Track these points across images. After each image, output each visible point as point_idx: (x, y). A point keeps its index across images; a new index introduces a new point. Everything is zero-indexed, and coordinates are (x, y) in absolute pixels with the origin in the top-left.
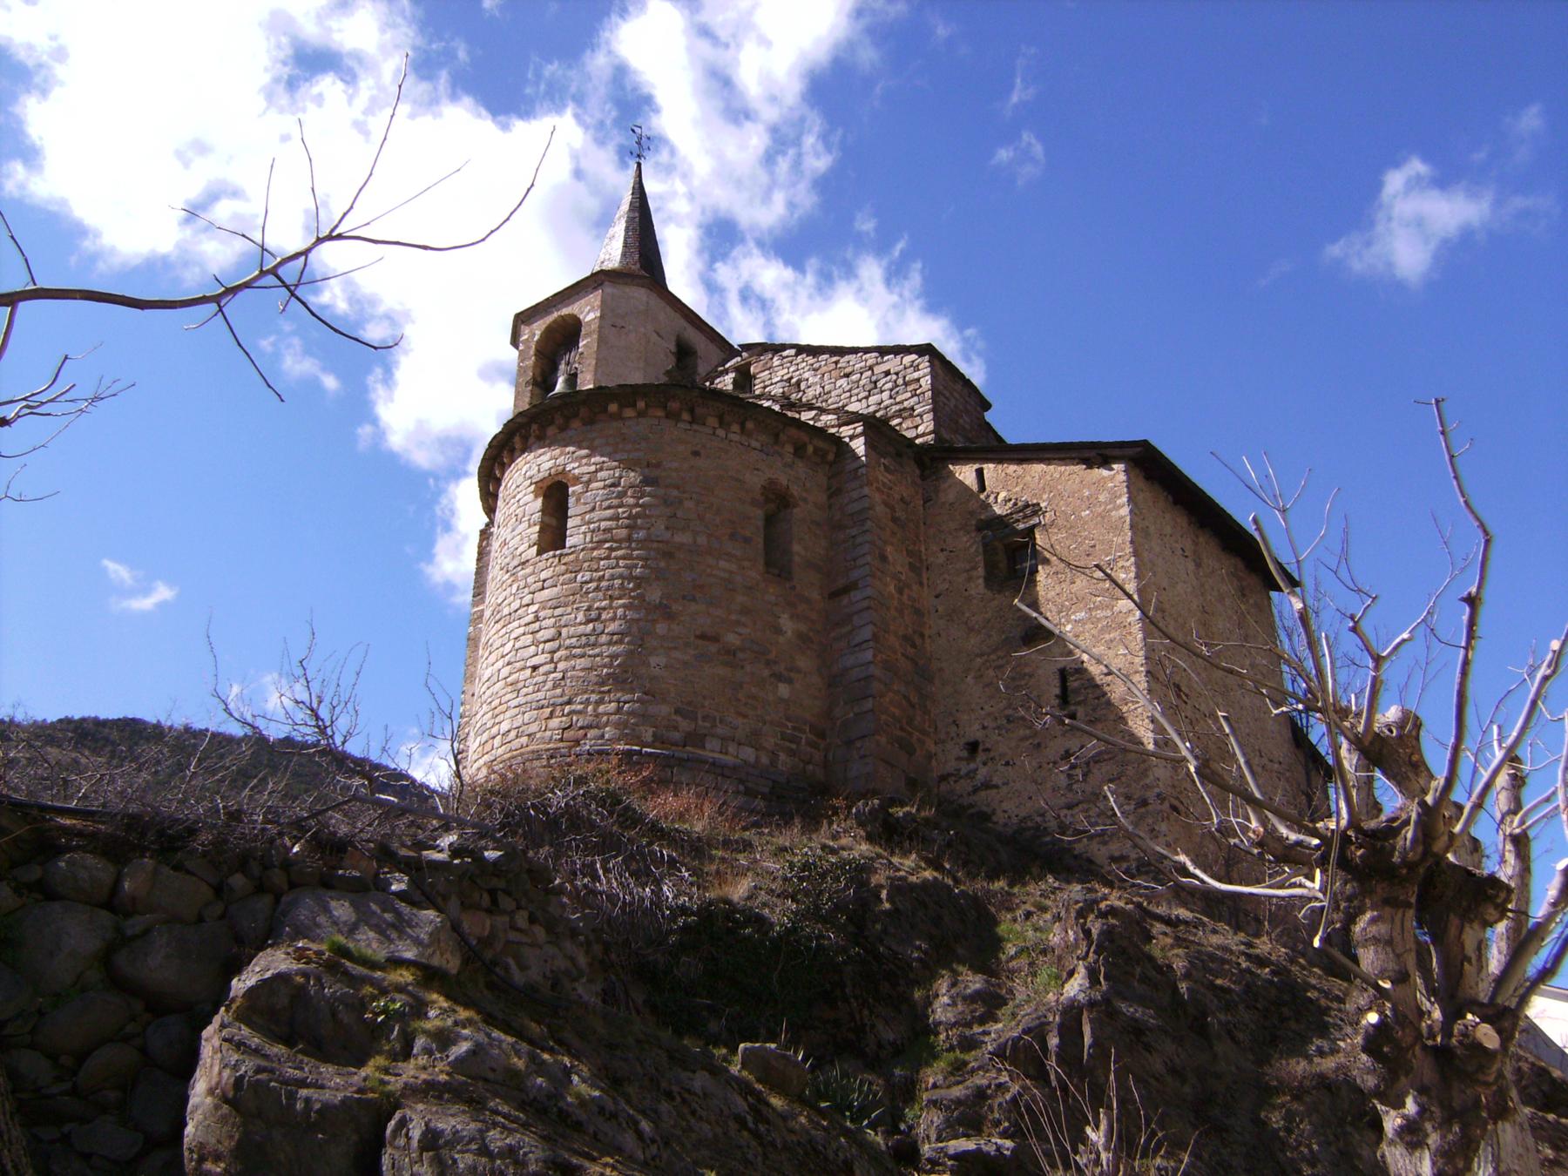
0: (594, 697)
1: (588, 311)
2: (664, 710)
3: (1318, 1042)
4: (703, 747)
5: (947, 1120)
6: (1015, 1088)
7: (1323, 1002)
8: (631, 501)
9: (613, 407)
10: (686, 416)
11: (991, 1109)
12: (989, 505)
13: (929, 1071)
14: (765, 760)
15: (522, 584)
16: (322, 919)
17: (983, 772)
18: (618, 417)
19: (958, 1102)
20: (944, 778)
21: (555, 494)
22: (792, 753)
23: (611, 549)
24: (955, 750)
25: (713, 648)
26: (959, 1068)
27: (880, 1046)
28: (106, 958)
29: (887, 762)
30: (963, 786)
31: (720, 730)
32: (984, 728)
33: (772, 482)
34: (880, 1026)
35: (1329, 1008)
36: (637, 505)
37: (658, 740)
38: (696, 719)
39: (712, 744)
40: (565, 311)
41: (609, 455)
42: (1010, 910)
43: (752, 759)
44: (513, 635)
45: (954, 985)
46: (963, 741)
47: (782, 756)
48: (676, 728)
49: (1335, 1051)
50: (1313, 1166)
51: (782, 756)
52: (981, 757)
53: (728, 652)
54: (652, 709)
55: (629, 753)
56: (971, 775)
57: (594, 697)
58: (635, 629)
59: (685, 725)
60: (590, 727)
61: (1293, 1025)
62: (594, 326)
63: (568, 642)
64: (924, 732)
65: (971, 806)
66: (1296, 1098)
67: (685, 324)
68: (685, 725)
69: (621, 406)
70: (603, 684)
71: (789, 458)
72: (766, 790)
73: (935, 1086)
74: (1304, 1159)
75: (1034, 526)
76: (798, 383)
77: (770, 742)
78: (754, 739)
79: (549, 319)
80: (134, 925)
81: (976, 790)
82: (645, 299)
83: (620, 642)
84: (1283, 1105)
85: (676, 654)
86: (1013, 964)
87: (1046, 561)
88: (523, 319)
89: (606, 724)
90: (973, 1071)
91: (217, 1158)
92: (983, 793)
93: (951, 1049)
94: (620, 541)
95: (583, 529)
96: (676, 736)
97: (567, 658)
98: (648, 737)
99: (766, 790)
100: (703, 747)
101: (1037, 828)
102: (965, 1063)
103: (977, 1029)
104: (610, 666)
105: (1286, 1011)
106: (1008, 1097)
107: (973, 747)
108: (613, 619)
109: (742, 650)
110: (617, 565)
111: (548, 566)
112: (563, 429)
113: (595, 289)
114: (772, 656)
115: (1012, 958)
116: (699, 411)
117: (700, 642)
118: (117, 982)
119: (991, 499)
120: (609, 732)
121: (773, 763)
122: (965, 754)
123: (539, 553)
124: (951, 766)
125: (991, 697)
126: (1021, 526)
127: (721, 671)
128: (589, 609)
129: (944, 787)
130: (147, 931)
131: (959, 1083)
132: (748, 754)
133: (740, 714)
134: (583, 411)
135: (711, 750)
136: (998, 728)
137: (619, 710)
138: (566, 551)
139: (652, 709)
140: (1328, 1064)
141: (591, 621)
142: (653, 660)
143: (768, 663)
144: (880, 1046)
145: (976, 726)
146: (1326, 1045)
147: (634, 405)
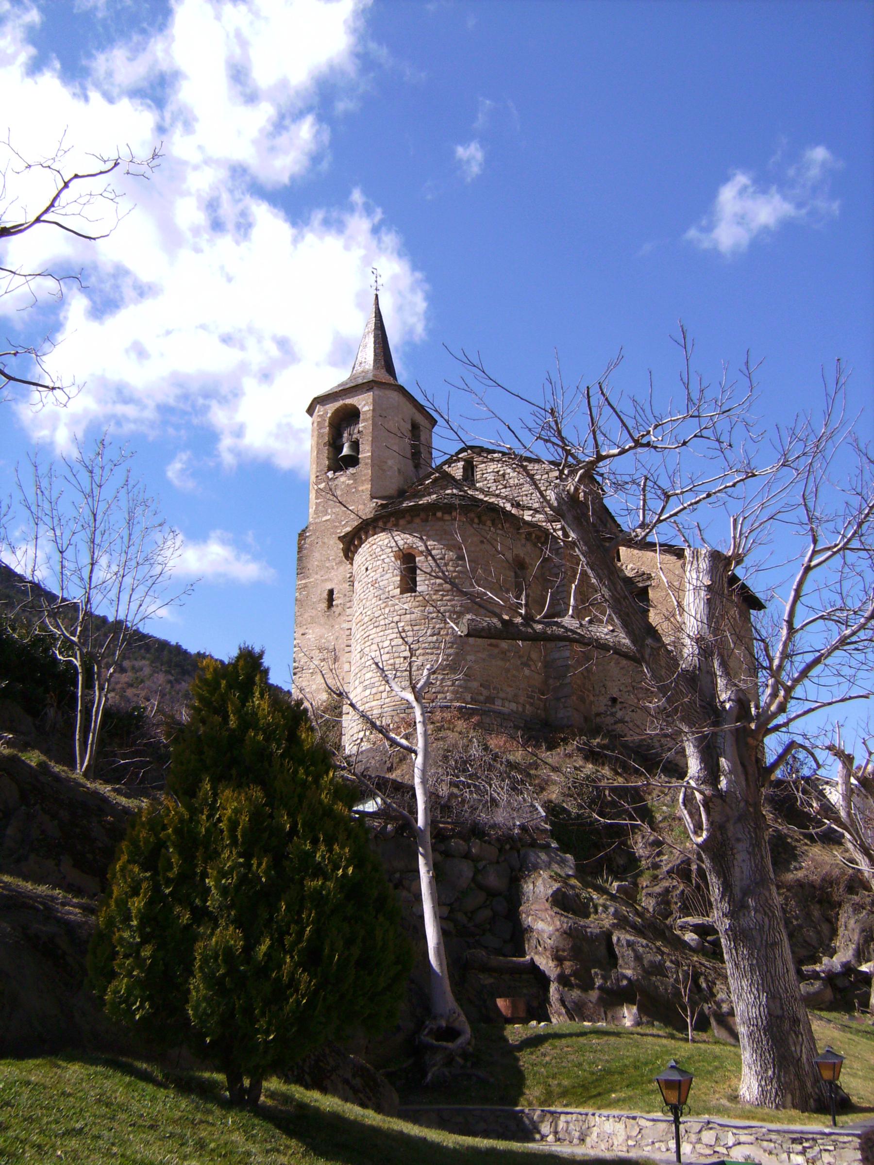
0: (440, 677)
1: (364, 403)
2: (475, 685)
3: (794, 864)
4: (494, 704)
5: (657, 902)
6: (681, 887)
7: (794, 844)
8: (452, 569)
9: (439, 514)
10: (476, 521)
11: (672, 897)
12: (622, 570)
13: (642, 879)
14: (520, 709)
15: (392, 609)
16: (539, 860)
17: (619, 714)
18: (442, 519)
19: (659, 894)
20: (598, 715)
21: (408, 563)
22: (531, 704)
23: (443, 595)
24: (604, 701)
25: (496, 651)
26: (655, 877)
27: (618, 867)
28: (474, 879)
29: (576, 710)
30: (610, 720)
31: (501, 695)
32: (620, 691)
33: (517, 556)
34: (618, 858)
35: (796, 847)
36: (455, 571)
37: (474, 701)
38: (489, 689)
39: (498, 702)
40: (348, 401)
41: (438, 541)
42: (650, 794)
43: (515, 709)
44: (389, 638)
45: (643, 837)
46: (609, 696)
47: (528, 706)
48: (481, 694)
49: (801, 868)
50: (797, 920)
51: (528, 706)
52: (618, 706)
53: (502, 653)
54: (470, 684)
55: (460, 708)
56: (613, 714)
57: (440, 677)
58: (458, 641)
59: (485, 693)
60: (439, 692)
61: (783, 855)
62: (370, 415)
63: (423, 645)
64: (589, 691)
65: (613, 730)
66: (788, 890)
67: (414, 410)
68: (485, 693)
69: (443, 513)
70: (444, 670)
71: (523, 541)
72: (522, 725)
73: (647, 886)
74: (793, 917)
75: (648, 586)
76: (504, 475)
77: (522, 699)
78: (515, 699)
79: (339, 403)
80: (480, 865)
81: (616, 723)
82: (397, 399)
83: (451, 647)
84: (783, 893)
85: (480, 655)
86: (661, 825)
87: (655, 607)
88: (320, 401)
89: (447, 691)
90: (662, 879)
91: (564, 950)
92: (620, 725)
93: (648, 869)
94: (448, 591)
95: (427, 582)
96: (482, 698)
97: (423, 655)
98: (468, 699)
99: (522, 725)
100: (494, 704)
101: (648, 746)
102: (658, 876)
103: (657, 859)
104: (447, 660)
105: (780, 849)
106: (678, 892)
107: (614, 700)
108: (447, 634)
109: (509, 651)
110: (447, 605)
111: (407, 602)
112: (409, 522)
113: (368, 390)
114: (521, 653)
115: (660, 822)
116: (484, 518)
117: (489, 648)
118: (480, 887)
119: (624, 567)
120: (449, 696)
121: (524, 711)
122: (610, 703)
123: (402, 593)
124: (602, 709)
125: (624, 675)
126: (641, 585)
127: (500, 663)
128: (434, 628)
129: (598, 719)
130: (484, 867)
131: (656, 885)
132: (513, 706)
133: (509, 686)
134: (423, 515)
135: (498, 706)
136: (628, 691)
137: (453, 685)
138: (417, 593)
139: (470, 684)
140: (800, 874)
141: (435, 635)
142: (469, 658)
143: (520, 657)
144: (618, 867)
145: (616, 689)
146: (798, 865)
147: (451, 513)
